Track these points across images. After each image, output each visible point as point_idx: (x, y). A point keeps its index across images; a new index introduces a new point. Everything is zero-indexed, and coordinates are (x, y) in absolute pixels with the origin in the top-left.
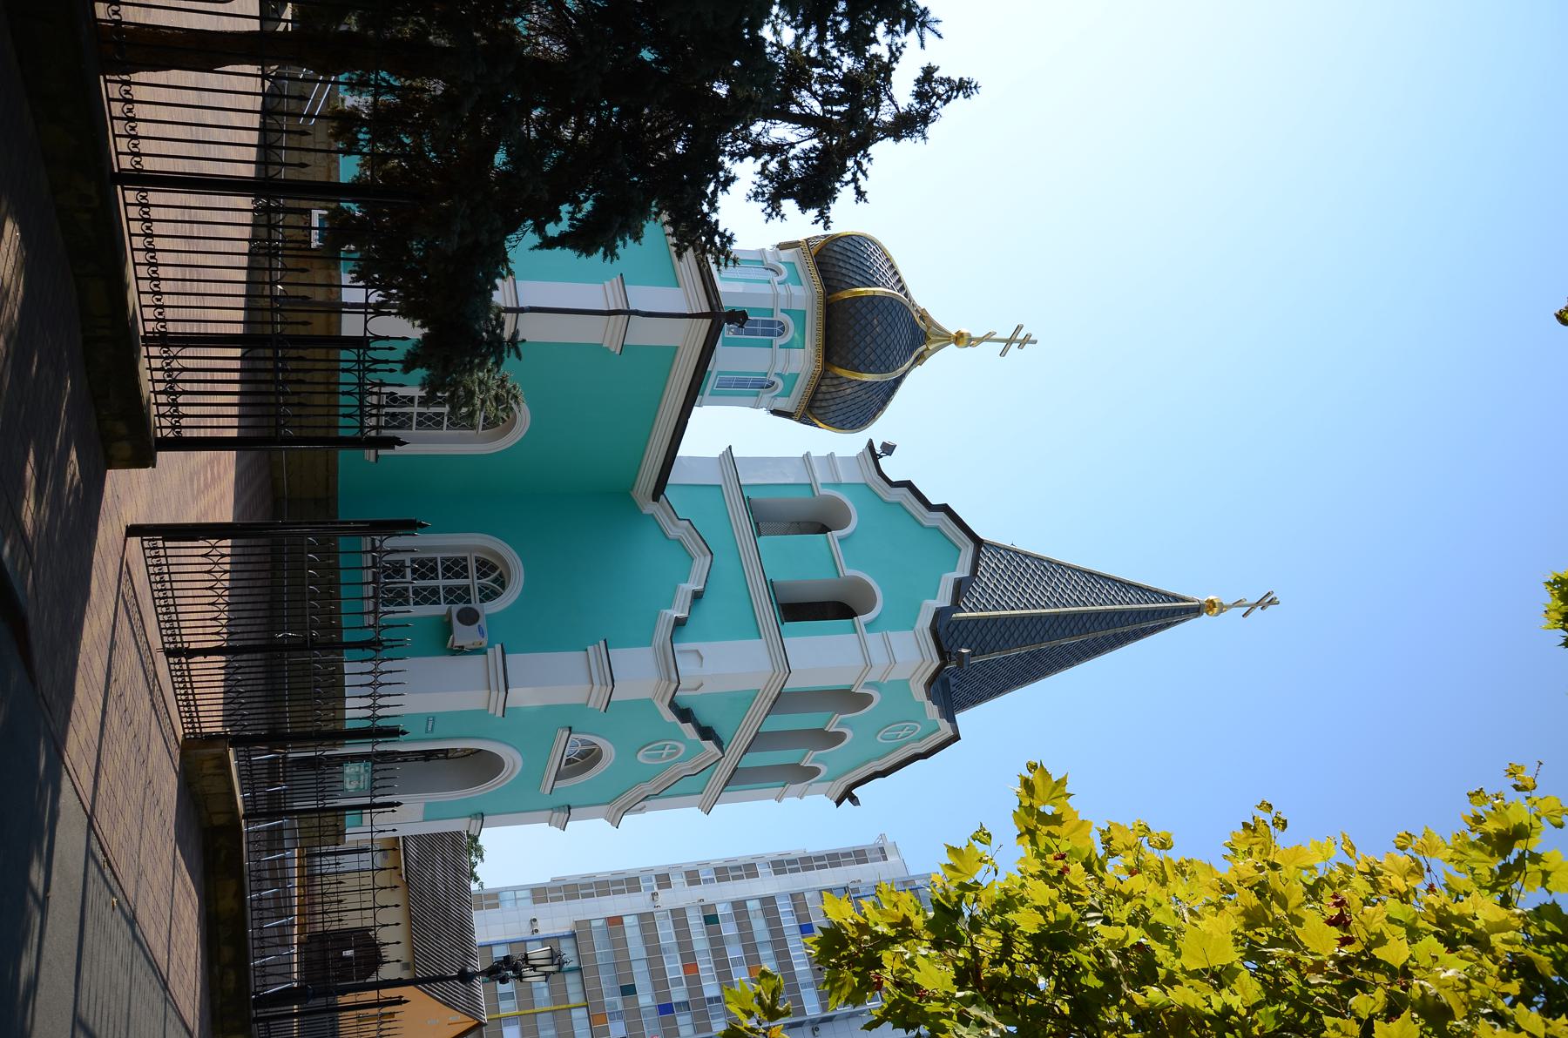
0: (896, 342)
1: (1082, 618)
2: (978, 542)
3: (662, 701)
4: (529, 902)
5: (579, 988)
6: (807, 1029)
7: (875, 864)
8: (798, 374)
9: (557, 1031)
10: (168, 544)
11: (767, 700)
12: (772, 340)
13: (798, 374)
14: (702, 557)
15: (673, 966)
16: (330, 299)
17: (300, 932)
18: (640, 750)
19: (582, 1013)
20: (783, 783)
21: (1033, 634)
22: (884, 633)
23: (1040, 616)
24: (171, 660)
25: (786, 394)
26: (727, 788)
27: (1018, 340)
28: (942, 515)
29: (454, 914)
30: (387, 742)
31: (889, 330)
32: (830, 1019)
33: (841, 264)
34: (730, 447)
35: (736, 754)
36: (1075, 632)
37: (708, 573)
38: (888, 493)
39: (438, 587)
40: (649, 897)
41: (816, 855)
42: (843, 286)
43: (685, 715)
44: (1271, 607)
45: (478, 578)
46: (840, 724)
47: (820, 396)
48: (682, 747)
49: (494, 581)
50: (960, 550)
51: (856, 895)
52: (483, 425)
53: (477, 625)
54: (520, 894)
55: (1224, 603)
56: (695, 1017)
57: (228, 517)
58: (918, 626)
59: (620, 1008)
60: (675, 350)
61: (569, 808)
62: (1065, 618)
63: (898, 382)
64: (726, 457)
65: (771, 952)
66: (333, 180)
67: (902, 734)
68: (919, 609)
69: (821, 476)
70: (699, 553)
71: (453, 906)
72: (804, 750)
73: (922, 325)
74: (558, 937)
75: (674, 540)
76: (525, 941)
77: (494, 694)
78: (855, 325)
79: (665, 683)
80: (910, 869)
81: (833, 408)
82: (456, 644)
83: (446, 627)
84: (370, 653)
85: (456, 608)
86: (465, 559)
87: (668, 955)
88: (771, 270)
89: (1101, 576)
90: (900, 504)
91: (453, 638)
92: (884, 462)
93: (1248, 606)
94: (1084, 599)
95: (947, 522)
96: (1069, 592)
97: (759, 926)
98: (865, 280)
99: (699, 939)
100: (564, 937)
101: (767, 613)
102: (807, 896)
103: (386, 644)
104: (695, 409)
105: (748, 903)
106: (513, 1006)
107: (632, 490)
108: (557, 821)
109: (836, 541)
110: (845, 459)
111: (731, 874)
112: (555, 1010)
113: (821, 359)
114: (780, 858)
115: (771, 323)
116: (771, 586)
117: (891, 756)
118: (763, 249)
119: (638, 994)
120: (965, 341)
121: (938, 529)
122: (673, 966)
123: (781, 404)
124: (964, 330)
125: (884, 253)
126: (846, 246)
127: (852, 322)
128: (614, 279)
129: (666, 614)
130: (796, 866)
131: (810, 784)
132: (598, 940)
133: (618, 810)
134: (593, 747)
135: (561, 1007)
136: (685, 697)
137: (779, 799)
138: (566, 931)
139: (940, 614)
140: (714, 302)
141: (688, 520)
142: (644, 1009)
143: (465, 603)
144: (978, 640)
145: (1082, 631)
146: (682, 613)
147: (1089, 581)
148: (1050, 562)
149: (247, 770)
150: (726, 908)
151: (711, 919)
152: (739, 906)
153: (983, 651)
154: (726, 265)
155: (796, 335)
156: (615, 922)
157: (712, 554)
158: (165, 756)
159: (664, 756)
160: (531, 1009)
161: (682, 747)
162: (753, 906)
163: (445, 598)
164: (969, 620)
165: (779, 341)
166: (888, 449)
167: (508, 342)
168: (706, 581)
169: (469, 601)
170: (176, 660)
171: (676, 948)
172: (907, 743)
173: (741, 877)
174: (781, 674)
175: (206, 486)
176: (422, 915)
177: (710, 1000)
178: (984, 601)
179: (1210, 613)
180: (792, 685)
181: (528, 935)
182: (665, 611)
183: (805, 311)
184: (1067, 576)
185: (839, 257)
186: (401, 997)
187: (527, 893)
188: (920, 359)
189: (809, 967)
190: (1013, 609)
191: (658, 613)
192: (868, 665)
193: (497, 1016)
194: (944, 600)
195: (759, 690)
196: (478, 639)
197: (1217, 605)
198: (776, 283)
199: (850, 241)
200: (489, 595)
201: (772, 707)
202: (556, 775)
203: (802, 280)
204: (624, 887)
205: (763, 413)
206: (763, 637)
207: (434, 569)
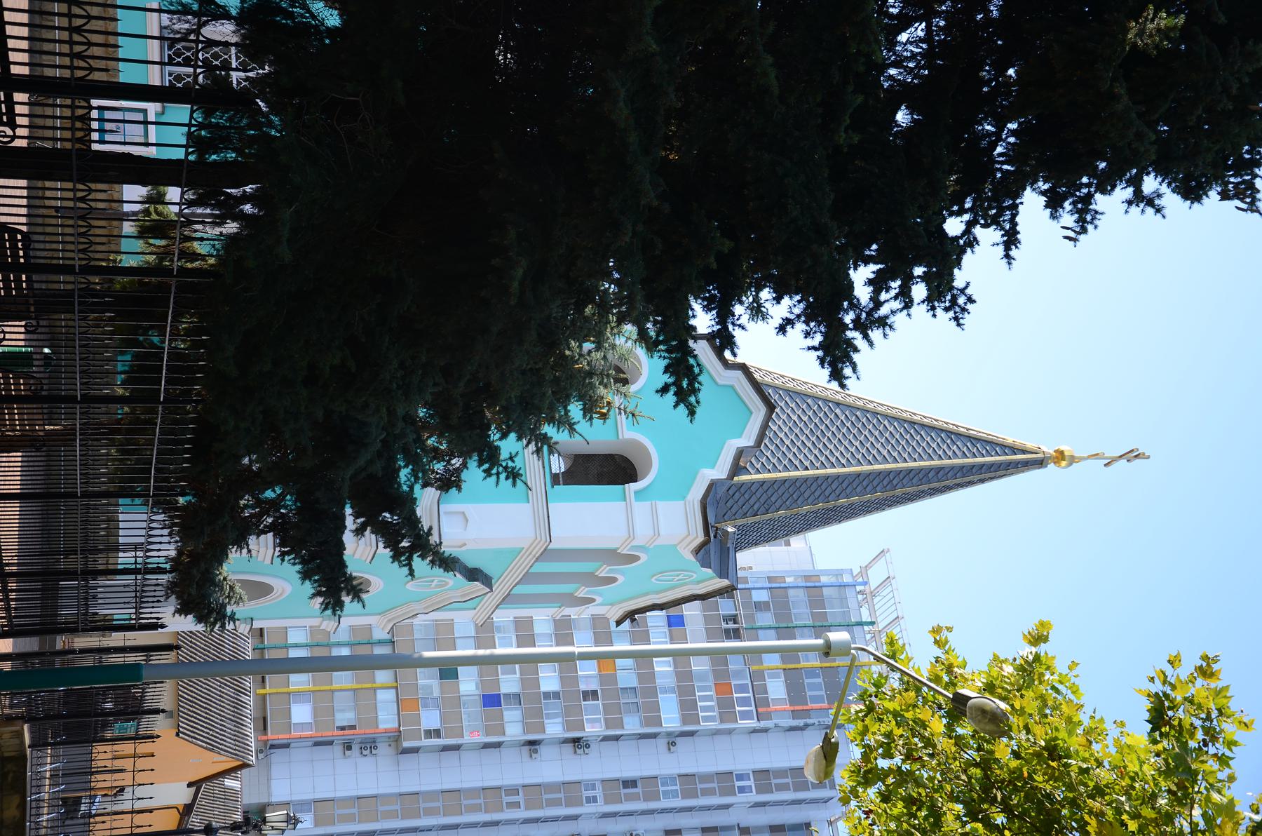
6: (662, 743)
11: (530, 557)
19: (391, 694)
20: (559, 605)
22: (653, 502)
32: (691, 734)
35: (506, 587)
50: (751, 413)
56: (526, 714)
58: (689, 497)
59: (436, 694)
67: (677, 578)
87: (501, 635)
93: (1106, 458)
119: (460, 679)
133: (389, 621)
142: (465, 698)
153: (767, 510)
164: (753, 483)
171: (512, 627)
172: (685, 584)
177: (547, 695)
189: (671, 669)
193: (285, 690)
197: (1067, 459)
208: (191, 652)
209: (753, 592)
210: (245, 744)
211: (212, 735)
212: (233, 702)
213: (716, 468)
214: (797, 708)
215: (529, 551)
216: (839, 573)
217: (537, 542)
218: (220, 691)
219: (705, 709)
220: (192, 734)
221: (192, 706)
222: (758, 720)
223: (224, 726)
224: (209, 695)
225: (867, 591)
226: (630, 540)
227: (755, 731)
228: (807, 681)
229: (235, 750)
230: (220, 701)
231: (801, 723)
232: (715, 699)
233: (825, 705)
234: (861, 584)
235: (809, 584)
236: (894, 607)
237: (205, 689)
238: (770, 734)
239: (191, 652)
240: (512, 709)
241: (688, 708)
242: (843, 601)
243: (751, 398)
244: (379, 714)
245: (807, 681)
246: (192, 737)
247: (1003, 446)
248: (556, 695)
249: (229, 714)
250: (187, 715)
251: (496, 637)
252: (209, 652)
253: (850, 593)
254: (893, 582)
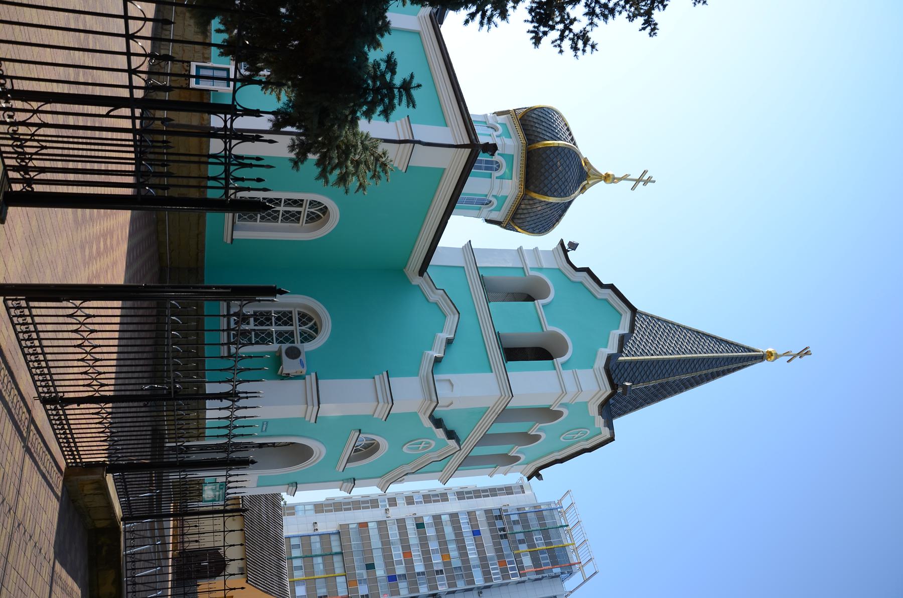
0: (571, 177)
1: (693, 361)
2: (633, 310)
3: (424, 414)
4: (313, 512)
5: (341, 564)
6: (475, 592)
7: (517, 495)
8: (507, 196)
9: (328, 589)
10: (32, 304)
12: (491, 174)
13: (507, 196)
14: (452, 316)
15: (397, 553)
16: (202, 124)
17: (174, 549)
18: (405, 444)
19: (343, 579)
20: (495, 465)
21: (664, 372)
22: (574, 370)
23: (669, 360)
24: (48, 407)
25: (499, 209)
26: (459, 468)
27: (644, 180)
28: (609, 291)
29: (272, 533)
30: (238, 468)
31: (567, 169)
32: (489, 587)
33: (537, 125)
34: (470, 241)
36: (689, 371)
37: (457, 326)
38: (574, 276)
40: (383, 511)
41: (483, 489)
42: (539, 139)
43: (438, 423)
44: (806, 357)
45: (300, 326)
46: (539, 430)
47: (520, 211)
48: (433, 444)
49: (310, 328)
50: (621, 315)
51: (506, 514)
52: (306, 220)
53: (299, 359)
54: (307, 507)
55: (778, 354)
57: (120, 281)
58: (596, 366)
59: (365, 577)
60: (444, 169)
61: (354, 480)
62: (684, 361)
63: (570, 203)
64: (467, 248)
65: (455, 546)
66: (205, 101)
67: (577, 436)
68: (596, 355)
69: (530, 263)
70: (451, 313)
71: (272, 528)
72: (513, 445)
73: (586, 168)
74: (329, 534)
75: (433, 303)
76: (310, 536)
77: (310, 408)
78: (545, 165)
79: (427, 403)
80: (538, 499)
81: (528, 219)
82: (284, 372)
83: (277, 360)
84: (226, 403)
85: (285, 346)
86: (291, 312)
87: (394, 546)
88: (491, 128)
89: (704, 334)
90: (581, 283)
91: (283, 368)
92: (571, 254)
94: (695, 349)
95: (613, 296)
96: (685, 344)
97: (448, 530)
98: (552, 136)
99: (413, 537)
100: (333, 534)
101: (496, 355)
102: (477, 513)
103: (241, 395)
104: (452, 217)
105: (442, 517)
106: (301, 574)
107: (405, 268)
108: (346, 488)
109: (541, 307)
110: (528, 251)
111: (432, 499)
112: (327, 577)
113: (523, 187)
114: (462, 490)
116: (498, 336)
117: (568, 449)
118: (486, 115)
120: (611, 180)
121: (606, 300)
122: (397, 553)
123: (495, 216)
124: (610, 173)
125: (563, 120)
126: (540, 114)
127: (543, 163)
128: (403, 119)
129: (428, 354)
130: (471, 495)
131: (512, 467)
132: (353, 536)
133: (387, 481)
134: (374, 442)
135: (330, 575)
136: (440, 412)
137: (491, 475)
138: (334, 530)
139: (610, 358)
140: (473, 137)
141: (443, 290)
143: (290, 343)
144: (631, 375)
145: (694, 370)
146: (439, 353)
147: (697, 337)
148: (673, 324)
149: (123, 486)
150: (429, 519)
151: (420, 526)
152: (437, 518)
154: (584, 51)
155: (507, 170)
156: (363, 525)
157: (459, 313)
158: (45, 491)
159: (420, 448)
160: (312, 576)
161: (433, 444)
162: (445, 518)
163: (277, 339)
165: (496, 174)
166: (574, 246)
167: (399, 89)
168: (456, 331)
169: (293, 342)
170: (53, 407)
171: (399, 542)
172: (579, 442)
173: (438, 501)
174: (506, 398)
175: (99, 254)
176: (252, 536)
177: (419, 574)
178: (634, 349)
179: (769, 359)
180: (512, 404)
181: (311, 532)
182: (427, 352)
183: (513, 155)
184: (684, 334)
185: (535, 120)
187: (311, 507)
188: (584, 189)
189: (477, 556)
190: (652, 355)
191: (423, 354)
192: (564, 392)
194: (613, 349)
195: (489, 407)
196: (300, 369)
197: (773, 355)
198: (495, 136)
199: (542, 111)
200: (307, 338)
201: (496, 418)
202: (348, 460)
203: (511, 135)
204: (369, 505)
205: (480, 222)
206: (450, 124)
208: (252, 533)
209: (511, 516)
210: (285, 590)
211: (266, 584)
212: (277, 565)
213: (608, 347)
214: (537, 569)
215: (494, 409)
216: (549, 504)
217: (503, 397)
218: (269, 558)
219: (495, 574)
220: (255, 582)
221: (254, 565)
222: (520, 577)
223: (273, 579)
224: (263, 560)
225: (562, 511)
226: (563, 395)
227: (519, 582)
228: (540, 556)
229: (280, 593)
230: (269, 563)
231: (540, 576)
232: (499, 569)
233: (550, 567)
234: (559, 508)
235: (536, 510)
236: (576, 517)
237: (261, 555)
238: (526, 584)
239: (252, 533)
240: (402, 582)
241: (487, 574)
242: (553, 517)
243: (618, 304)
244: (338, 589)
245: (540, 556)
246: (256, 584)
247: (743, 347)
248: (423, 573)
249: (275, 572)
250: (252, 570)
251: (392, 547)
252: (262, 534)
253: (555, 512)
254: (574, 505)
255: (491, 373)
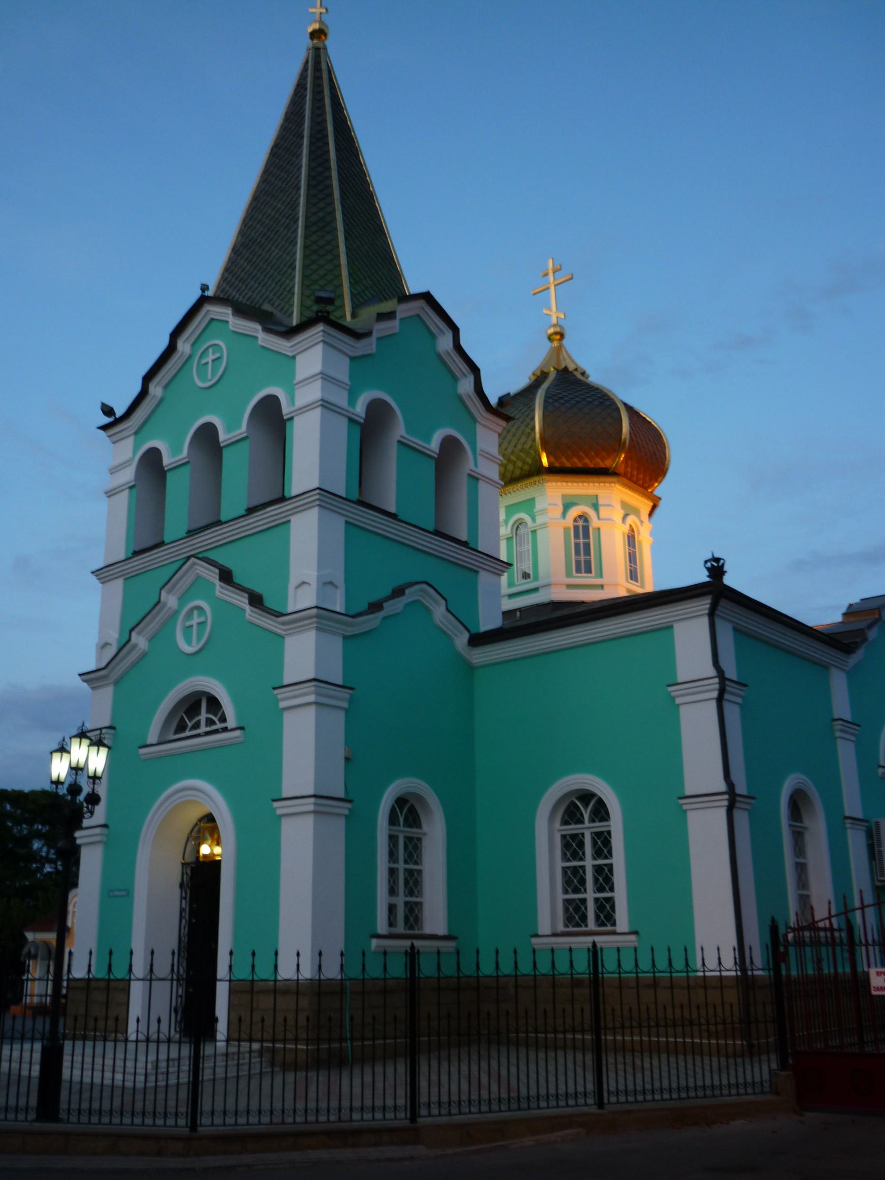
34: (92, 573)
39: (594, 866)
50: (212, 320)
86: (564, 837)
115: (576, 528)
163: (606, 858)
165: (594, 523)
166: (108, 411)
186: (589, 950)
207: (575, 870)
255: (292, 523)
